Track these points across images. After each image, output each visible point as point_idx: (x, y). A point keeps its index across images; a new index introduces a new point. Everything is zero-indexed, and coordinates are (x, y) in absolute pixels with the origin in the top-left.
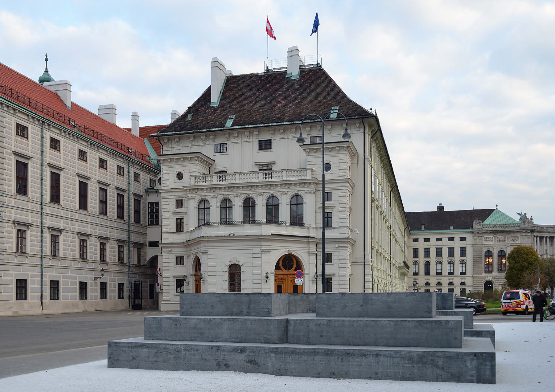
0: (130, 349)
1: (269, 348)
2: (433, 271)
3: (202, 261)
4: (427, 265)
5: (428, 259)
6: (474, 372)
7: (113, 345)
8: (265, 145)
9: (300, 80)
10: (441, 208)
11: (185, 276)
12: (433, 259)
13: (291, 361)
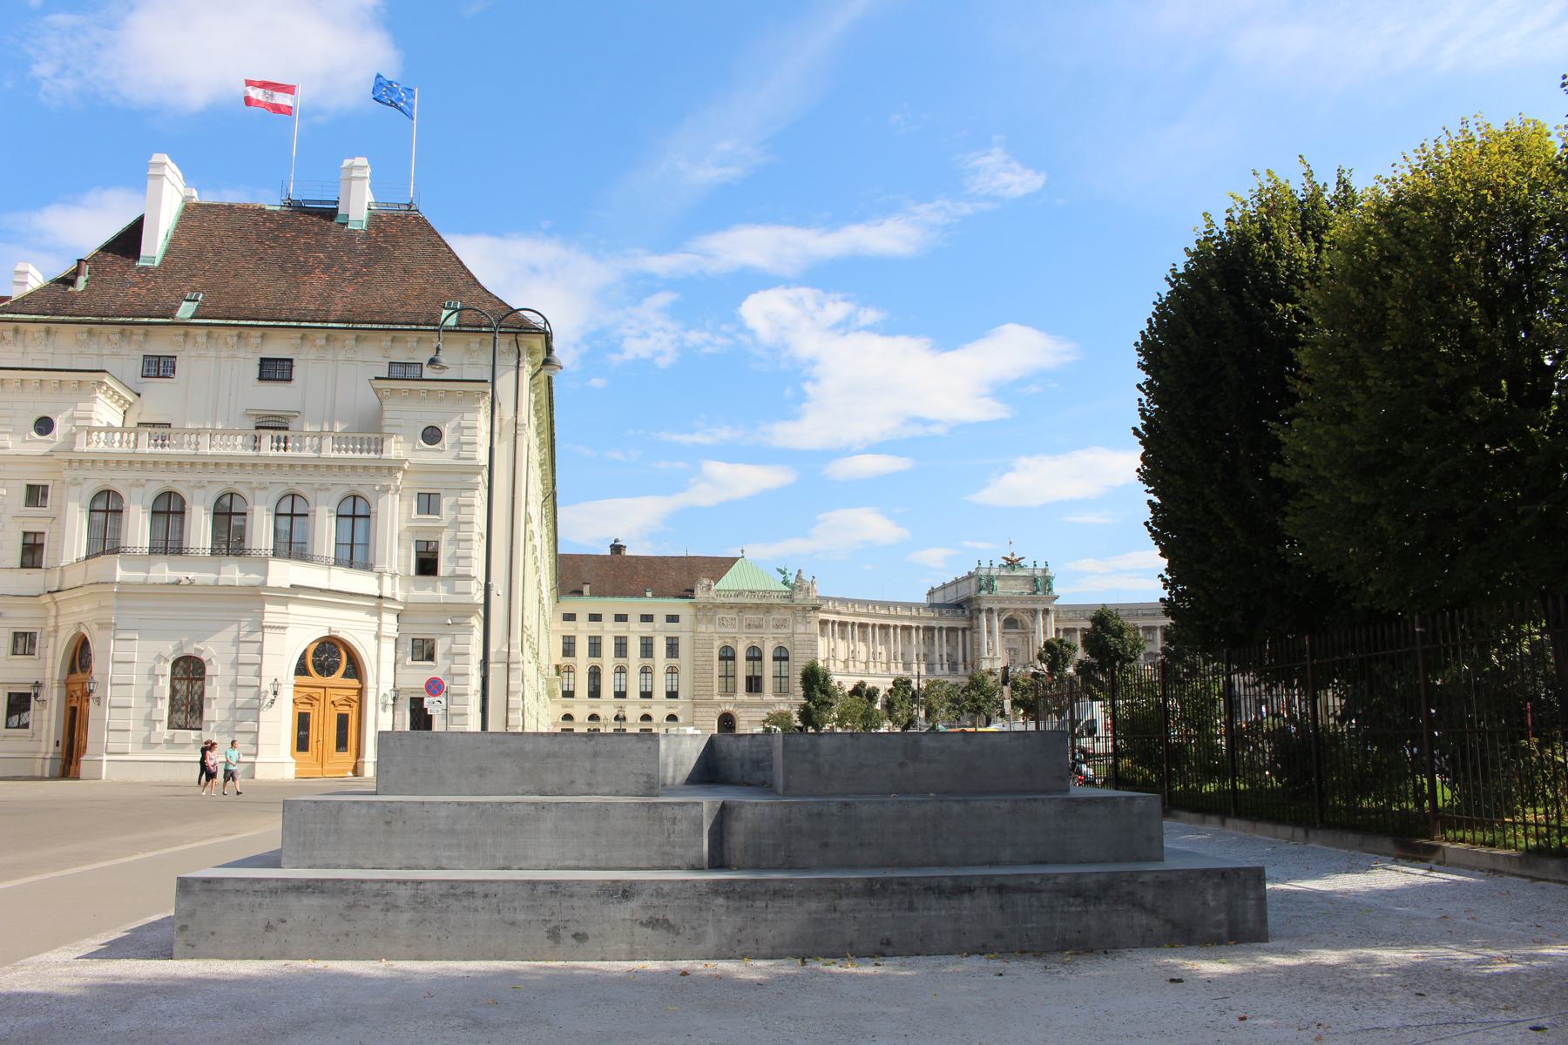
0: (259, 900)
1: (708, 882)
2: (608, 685)
3: (94, 647)
4: (595, 674)
5: (595, 661)
6: (1222, 916)
7: (197, 886)
8: (274, 370)
9: (368, 233)
10: (617, 548)
11: (38, 685)
12: (608, 661)
13: (770, 917)
